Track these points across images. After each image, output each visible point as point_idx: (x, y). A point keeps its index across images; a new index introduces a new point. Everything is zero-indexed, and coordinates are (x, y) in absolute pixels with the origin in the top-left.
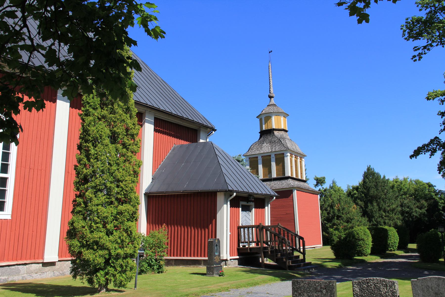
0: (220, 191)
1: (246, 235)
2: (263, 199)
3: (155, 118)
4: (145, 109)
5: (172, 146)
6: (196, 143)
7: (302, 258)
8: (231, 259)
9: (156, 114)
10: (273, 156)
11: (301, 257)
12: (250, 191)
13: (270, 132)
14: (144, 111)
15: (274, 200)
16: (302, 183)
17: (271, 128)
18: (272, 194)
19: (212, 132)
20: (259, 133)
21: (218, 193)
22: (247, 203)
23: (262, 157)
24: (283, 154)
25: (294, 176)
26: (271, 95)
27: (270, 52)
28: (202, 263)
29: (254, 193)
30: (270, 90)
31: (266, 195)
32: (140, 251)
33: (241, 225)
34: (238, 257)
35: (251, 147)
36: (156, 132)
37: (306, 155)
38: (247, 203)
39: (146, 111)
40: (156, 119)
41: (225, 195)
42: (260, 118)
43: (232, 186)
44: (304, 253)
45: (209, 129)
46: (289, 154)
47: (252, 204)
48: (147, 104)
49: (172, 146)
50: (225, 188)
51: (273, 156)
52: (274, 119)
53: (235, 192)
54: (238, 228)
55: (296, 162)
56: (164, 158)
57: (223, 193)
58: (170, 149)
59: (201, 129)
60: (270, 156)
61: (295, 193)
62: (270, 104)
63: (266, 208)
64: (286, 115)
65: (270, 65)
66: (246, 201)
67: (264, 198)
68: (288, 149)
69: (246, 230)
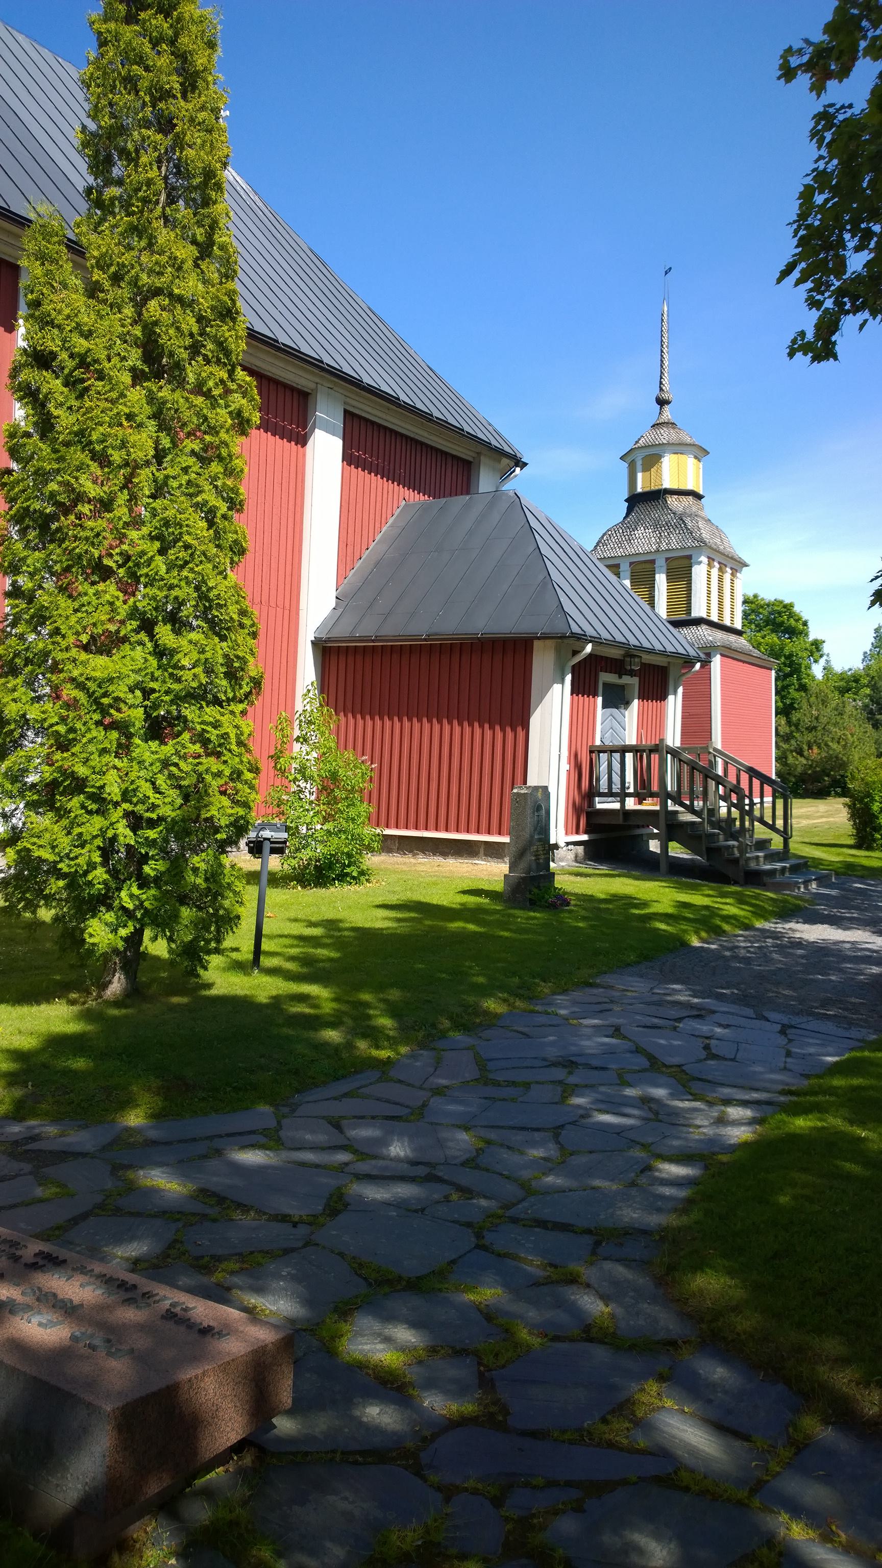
0: (545, 637)
1: (614, 774)
2: (662, 667)
3: (346, 413)
4: (317, 380)
5: (395, 505)
6: (468, 497)
7: (781, 847)
8: (568, 844)
9: (348, 400)
10: (661, 562)
11: (777, 843)
12: (633, 641)
13: (657, 496)
14: (313, 386)
15: (697, 672)
16: (732, 638)
17: (660, 487)
18: (692, 653)
19: (514, 471)
20: (626, 501)
21: (536, 644)
22: (620, 677)
23: (631, 564)
24: (689, 557)
25: (714, 618)
26: (665, 396)
27: (666, 273)
28: (482, 851)
29: (641, 649)
30: (661, 383)
31: (676, 655)
32: (273, 833)
33: (598, 742)
34: (585, 837)
35: (602, 537)
36: (349, 464)
37: (748, 562)
38: (620, 677)
39: (319, 386)
40: (349, 416)
41: (558, 650)
42: (629, 459)
43: (581, 623)
44: (786, 834)
45: (505, 461)
46: (704, 559)
47: (633, 682)
48: (322, 362)
49: (395, 505)
50: (560, 628)
51: (661, 562)
52: (668, 462)
53: (591, 642)
54: (591, 752)
55: (721, 580)
56: (371, 539)
57: (549, 643)
58: (389, 512)
59: (482, 458)
60: (653, 562)
61: (717, 662)
62: (661, 421)
63: (671, 698)
64: (700, 453)
65: (666, 309)
66: (615, 673)
67: (665, 665)
68: (702, 545)
69: (617, 756)
